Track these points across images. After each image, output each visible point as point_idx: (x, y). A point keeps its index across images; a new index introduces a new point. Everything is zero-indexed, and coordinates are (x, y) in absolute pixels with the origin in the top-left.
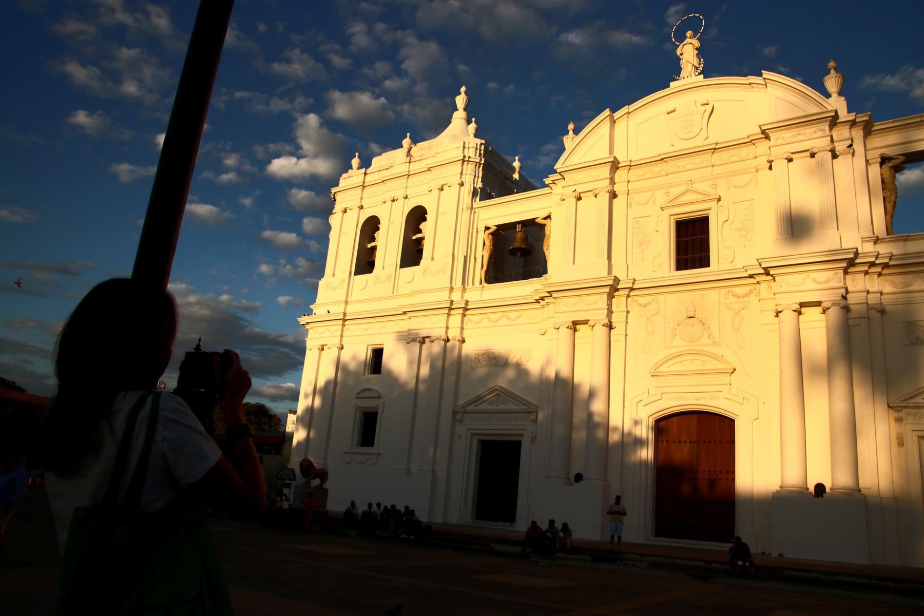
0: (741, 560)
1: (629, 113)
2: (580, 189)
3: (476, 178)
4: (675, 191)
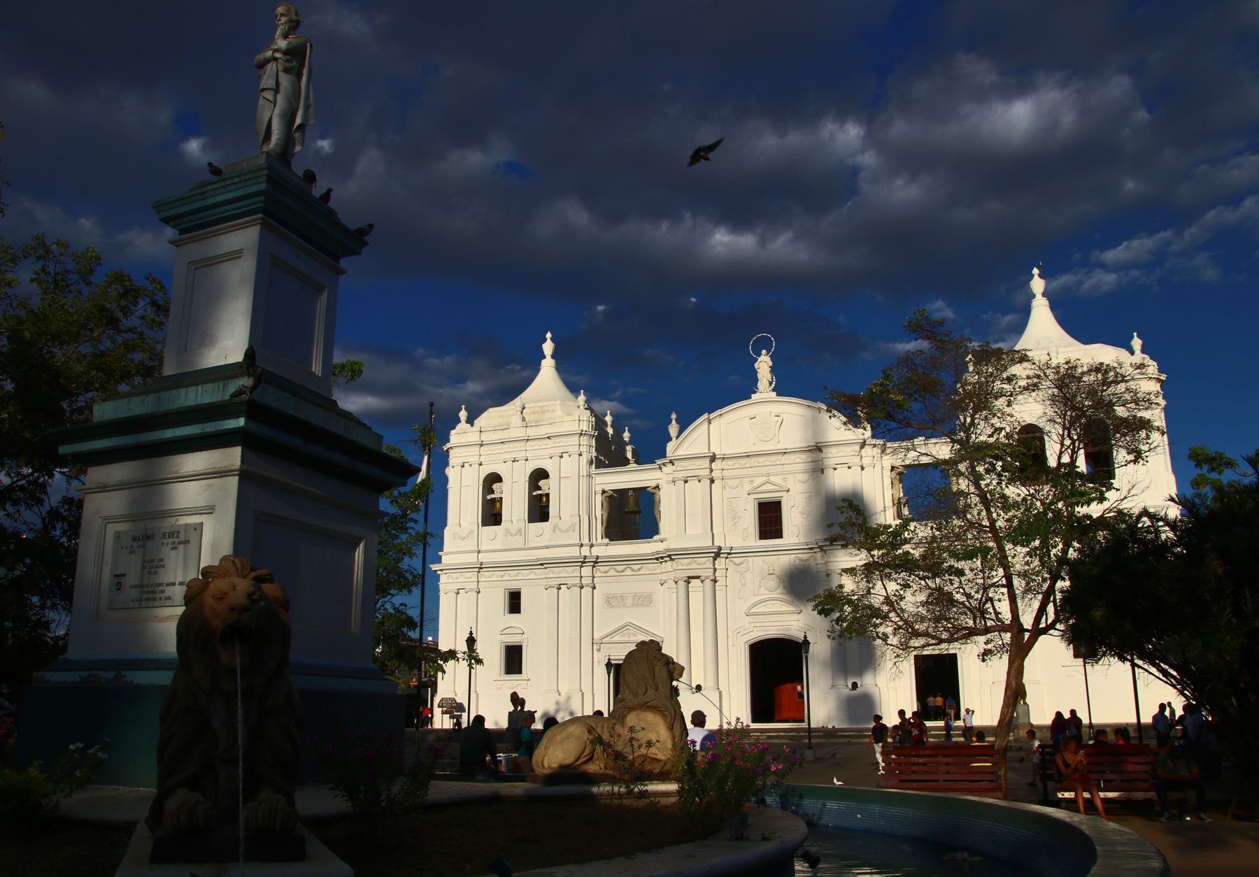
0: (601, 305)
3: (251, 175)
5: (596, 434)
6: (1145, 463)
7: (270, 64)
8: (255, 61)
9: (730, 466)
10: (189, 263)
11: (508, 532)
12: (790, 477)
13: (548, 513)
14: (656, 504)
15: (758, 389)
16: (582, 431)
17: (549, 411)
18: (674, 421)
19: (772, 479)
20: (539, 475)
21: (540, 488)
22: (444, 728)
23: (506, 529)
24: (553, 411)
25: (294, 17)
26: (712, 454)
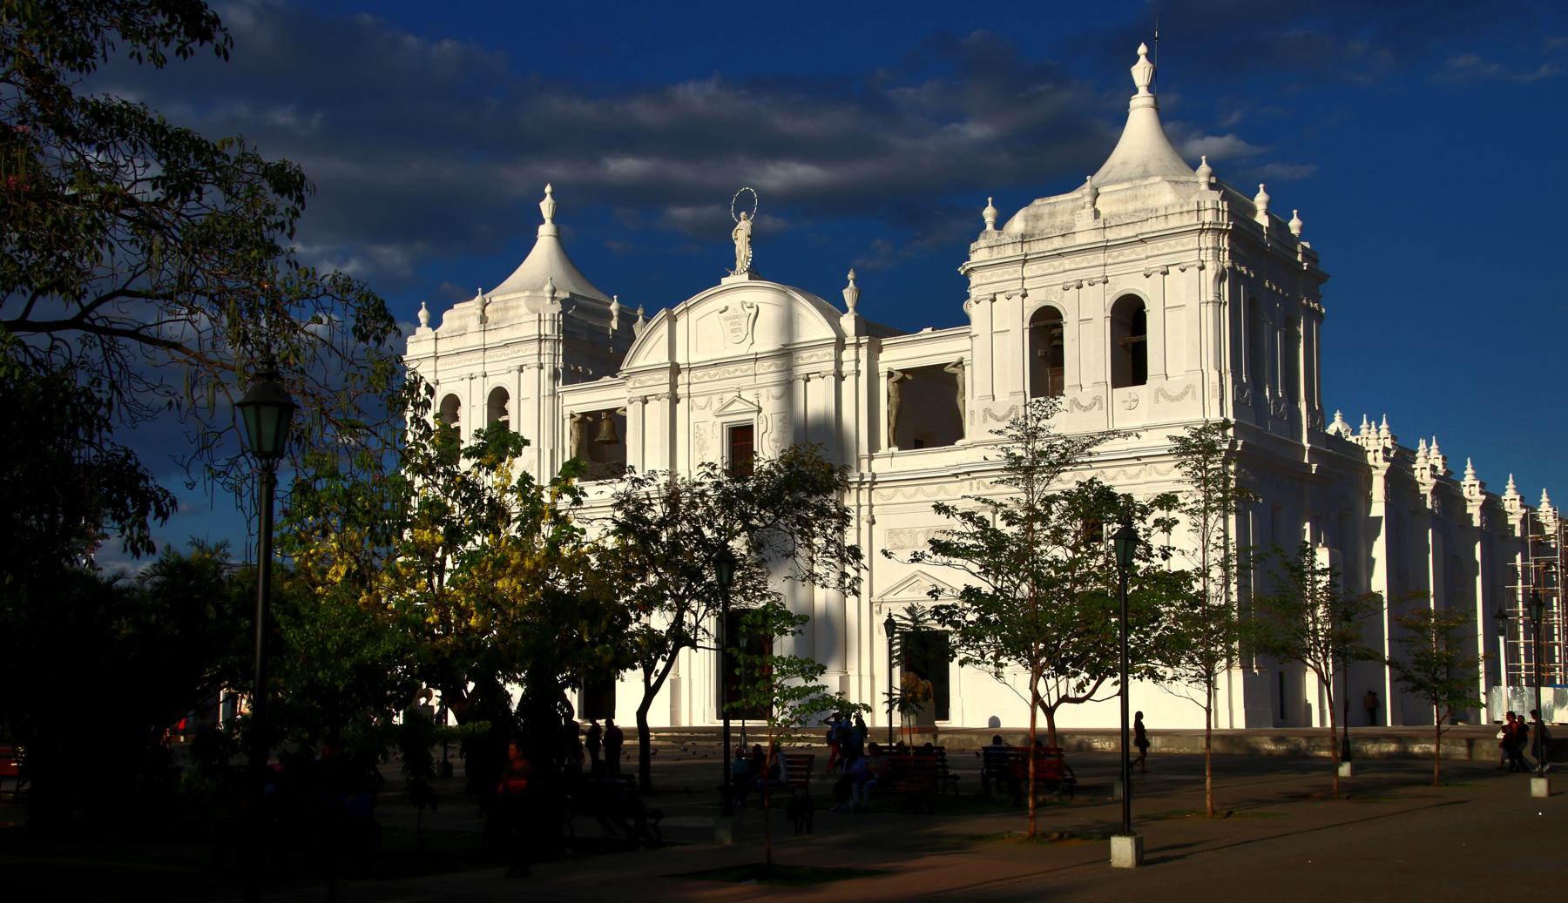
4: (728, 397)
12: (763, 392)
16: (1204, 224)
17: (512, 307)
22: (684, 723)
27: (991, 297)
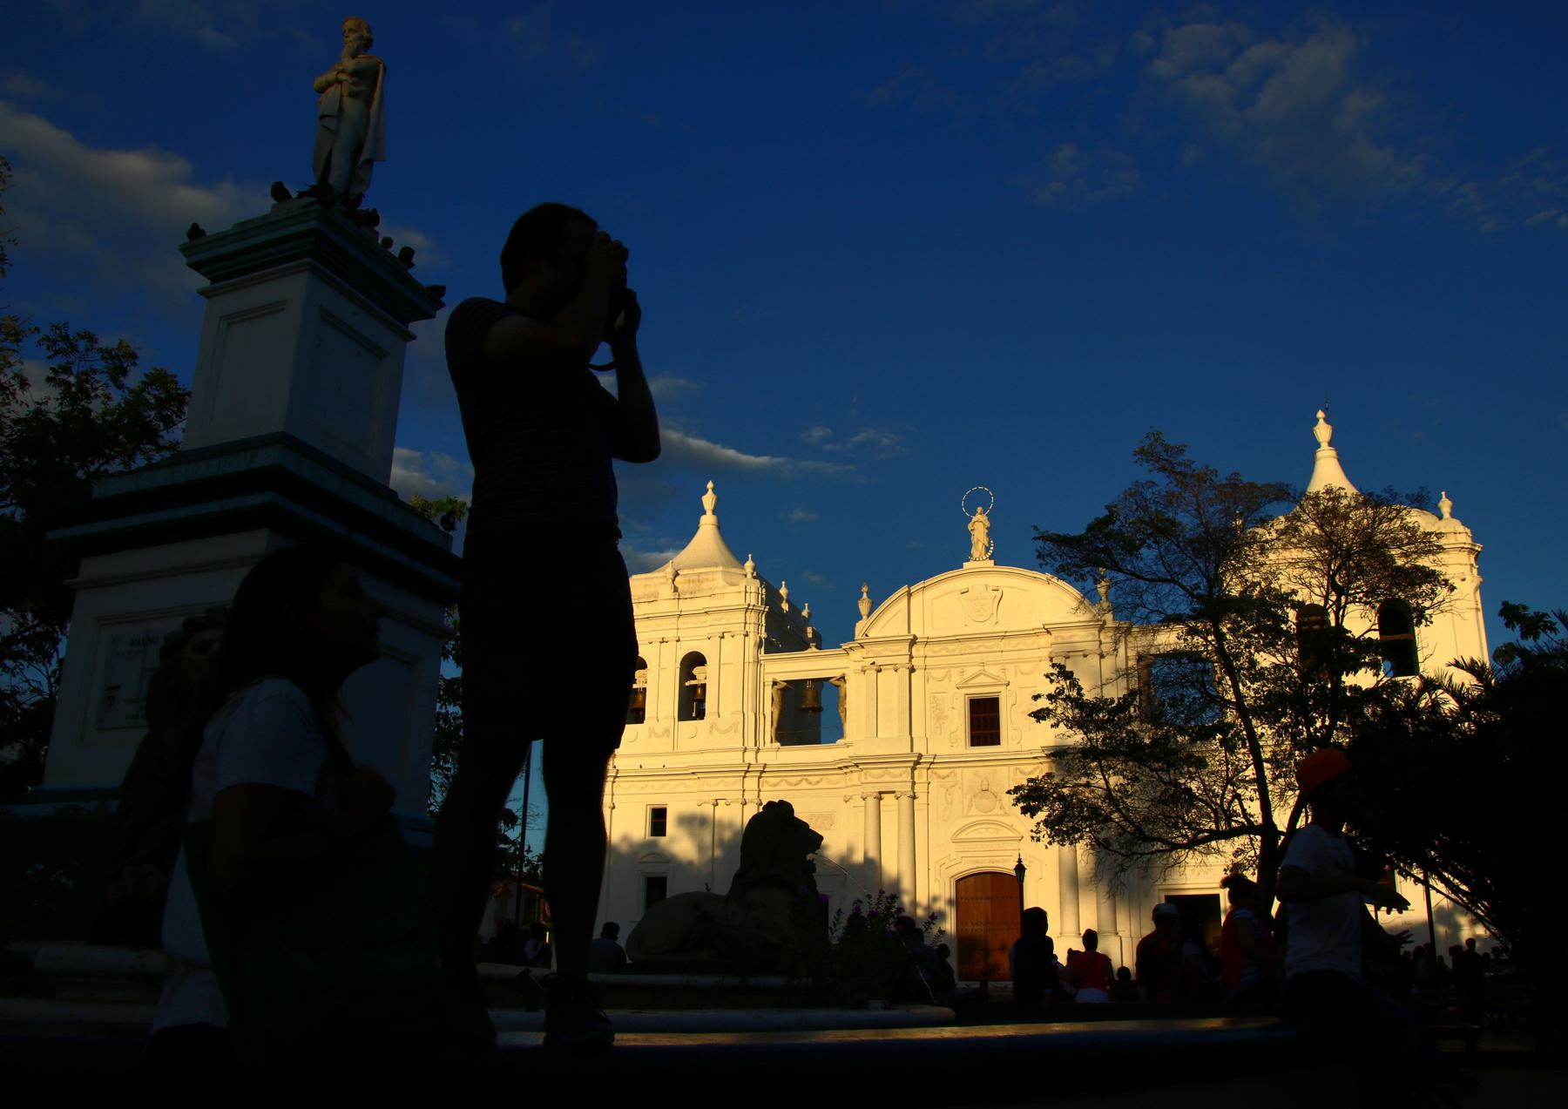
1: (924, 587)
2: (879, 661)
4: (970, 672)
5: (767, 610)
6: (1428, 623)
7: (334, 87)
8: (315, 85)
9: (934, 652)
10: (222, 317)
11: (652, 733)
13: (704, 710)
14: (841, 699)
15: (972, 556)
16: (749, 605)
17: (707, 580)
18: (865, 595)
19: (989, 669)
20: (694, 660)
21: (694, 678)
23: (650, 728)
24: (713, 580)
25: (366, 34)
26: (912, 637)
27: (721, 635)
